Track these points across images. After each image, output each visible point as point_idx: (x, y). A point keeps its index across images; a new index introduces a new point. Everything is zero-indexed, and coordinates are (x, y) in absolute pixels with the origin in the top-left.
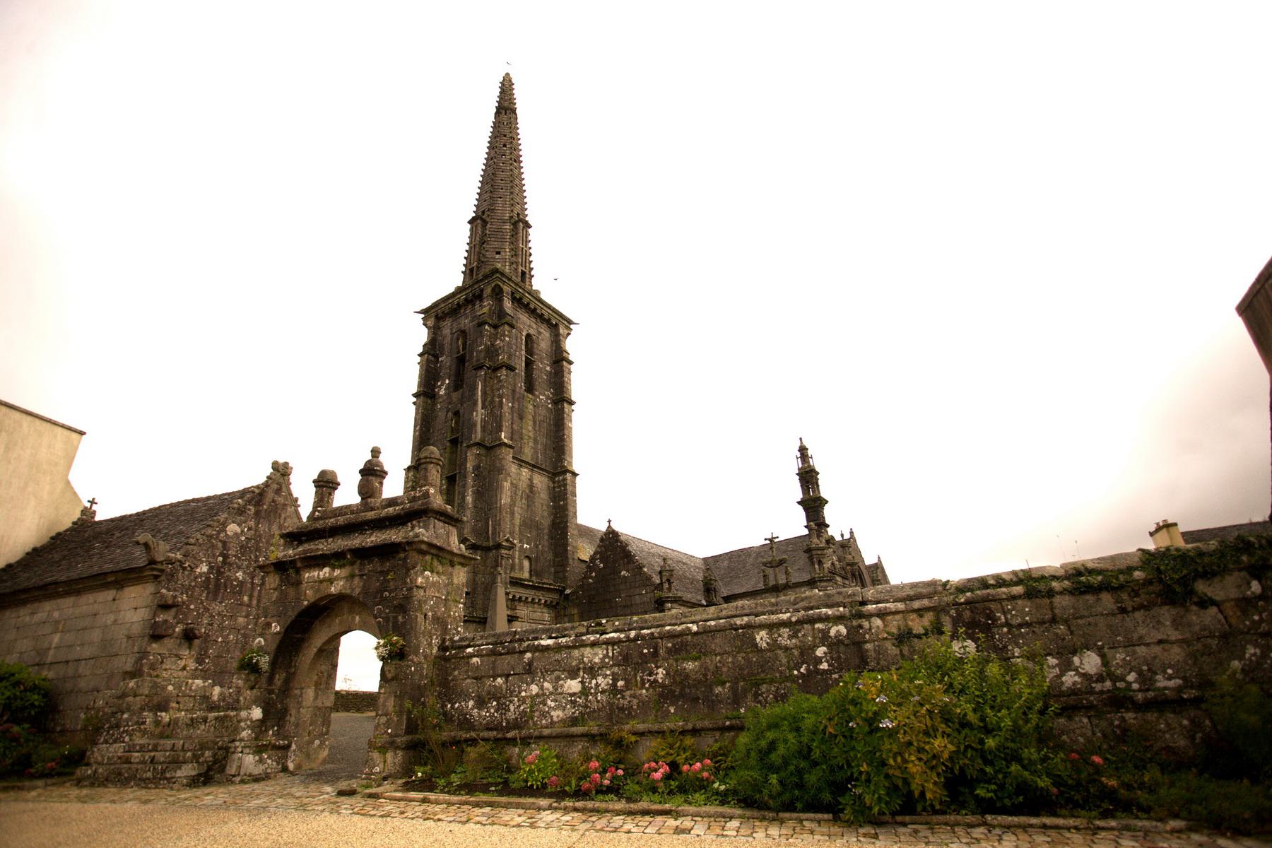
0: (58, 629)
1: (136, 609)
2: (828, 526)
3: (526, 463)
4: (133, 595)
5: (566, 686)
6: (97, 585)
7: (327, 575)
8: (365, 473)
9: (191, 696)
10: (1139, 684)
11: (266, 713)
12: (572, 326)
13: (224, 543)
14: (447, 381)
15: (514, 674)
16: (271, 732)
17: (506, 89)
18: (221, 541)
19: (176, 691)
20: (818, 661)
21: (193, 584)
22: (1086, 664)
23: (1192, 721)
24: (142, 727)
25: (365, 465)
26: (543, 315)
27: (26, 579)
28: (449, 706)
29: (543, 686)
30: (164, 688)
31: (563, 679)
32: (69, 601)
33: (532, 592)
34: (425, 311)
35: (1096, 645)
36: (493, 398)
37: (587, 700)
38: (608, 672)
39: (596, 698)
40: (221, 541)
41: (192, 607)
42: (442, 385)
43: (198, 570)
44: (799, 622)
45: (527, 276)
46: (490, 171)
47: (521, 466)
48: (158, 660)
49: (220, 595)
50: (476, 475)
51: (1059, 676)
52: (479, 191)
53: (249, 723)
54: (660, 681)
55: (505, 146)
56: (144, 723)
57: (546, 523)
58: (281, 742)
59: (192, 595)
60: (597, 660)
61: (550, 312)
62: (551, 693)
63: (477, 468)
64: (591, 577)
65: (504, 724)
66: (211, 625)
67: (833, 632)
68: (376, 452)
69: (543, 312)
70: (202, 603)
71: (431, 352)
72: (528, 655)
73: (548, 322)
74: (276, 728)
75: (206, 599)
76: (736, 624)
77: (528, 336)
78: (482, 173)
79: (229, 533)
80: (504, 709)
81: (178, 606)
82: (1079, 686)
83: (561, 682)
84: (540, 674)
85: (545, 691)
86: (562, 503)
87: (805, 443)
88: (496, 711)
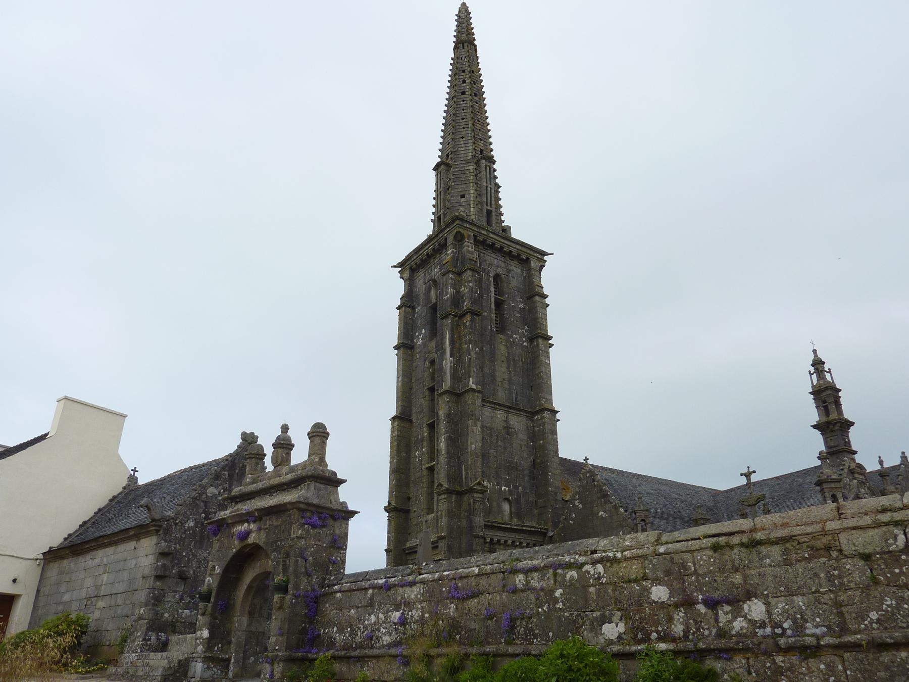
0: (106, 571)
1: (147, 555)
2: (855, 453)
3: (500, 405)
4: (145, 546)
5: (393, 616)
6: (125, 538)
7: (246, 528)
8: (275, 446)
9: (182, 622)
10: (793, 630)
11: (211, 633)
12: (546, 258)
13: (206, 503)
14: (423, 332)
15: (361, 607)
16: (216, 648)
17: (464, 18)
18: (203, 501)
19: (171, 618)
20: (556, 601)
21: (184, 536)
22: (753, 611)
23: (828, 666)
24: (149, 643)
25: (276, 440)
26: (510, 252)
27: (94, 533)
28: (322, 631)
29: (378, 616)
30: (162, 615)
31: (391, 611)
32: (110, 550)
33: (513, 535)
34: (401, 265)
35: (762, 594)
36: (460, 345)
38: (419, 606)
39: (411, 627)
40: (203, 501)
41: (184, 554)
42: (420, 335)
43: (187, 525)
44: (546, 567)
45: (494, 214)
46: (452, 111)
47: (495, 409)
48: (161, 594)
49: (205, 544)
50: (447, 422)
51: (730, 622)
52: (442, 134)
54: (452, 614)
55: (464, 82)
56: (150, 640)
57: (526, 464)
58: (223, 656)
59: (183, 544)
60: (413, 596)
61: (518, 247)
62: (384, 622)
63: (449, 415)
64: (572, 519)
65: (354, 645)
66: (199, 568)
67: (568, 577)
68: (285, 428)
69: (511, 249)
70: (191, 551)
71: (408, 304)
72: (370, 591)
73: (517, 258)
74: (220, 646)
75: (195, 547)
77: (497, 277)
78: (445, 115)
79: (208, 494)
80: (354, 634)
81: (172, 553)
82: (745, 631)
86: (541, 442)
87: (820, 355)
88: (350, 636)
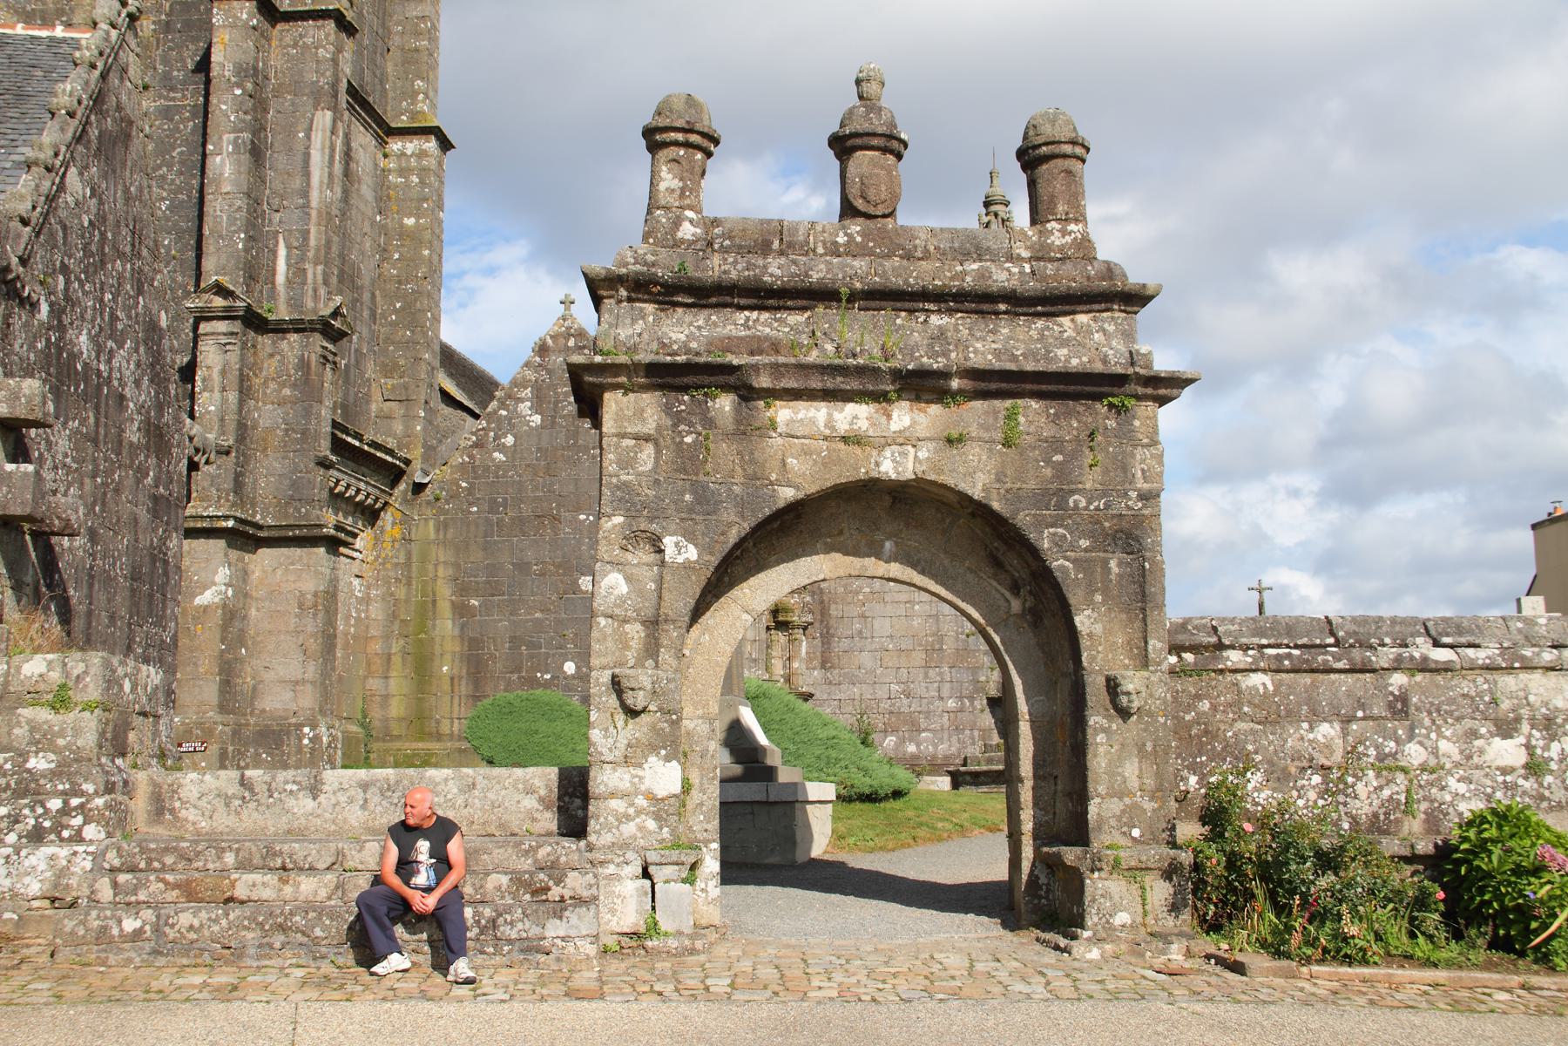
31: (1482, 737)
37: (1541, 785)
53: (641, 802)
62: (1457, 765)
64: (502, 448)
76: (1412, 658)
83: (1478, 743)
84: (1427, 722)
85: (1443, 760)
